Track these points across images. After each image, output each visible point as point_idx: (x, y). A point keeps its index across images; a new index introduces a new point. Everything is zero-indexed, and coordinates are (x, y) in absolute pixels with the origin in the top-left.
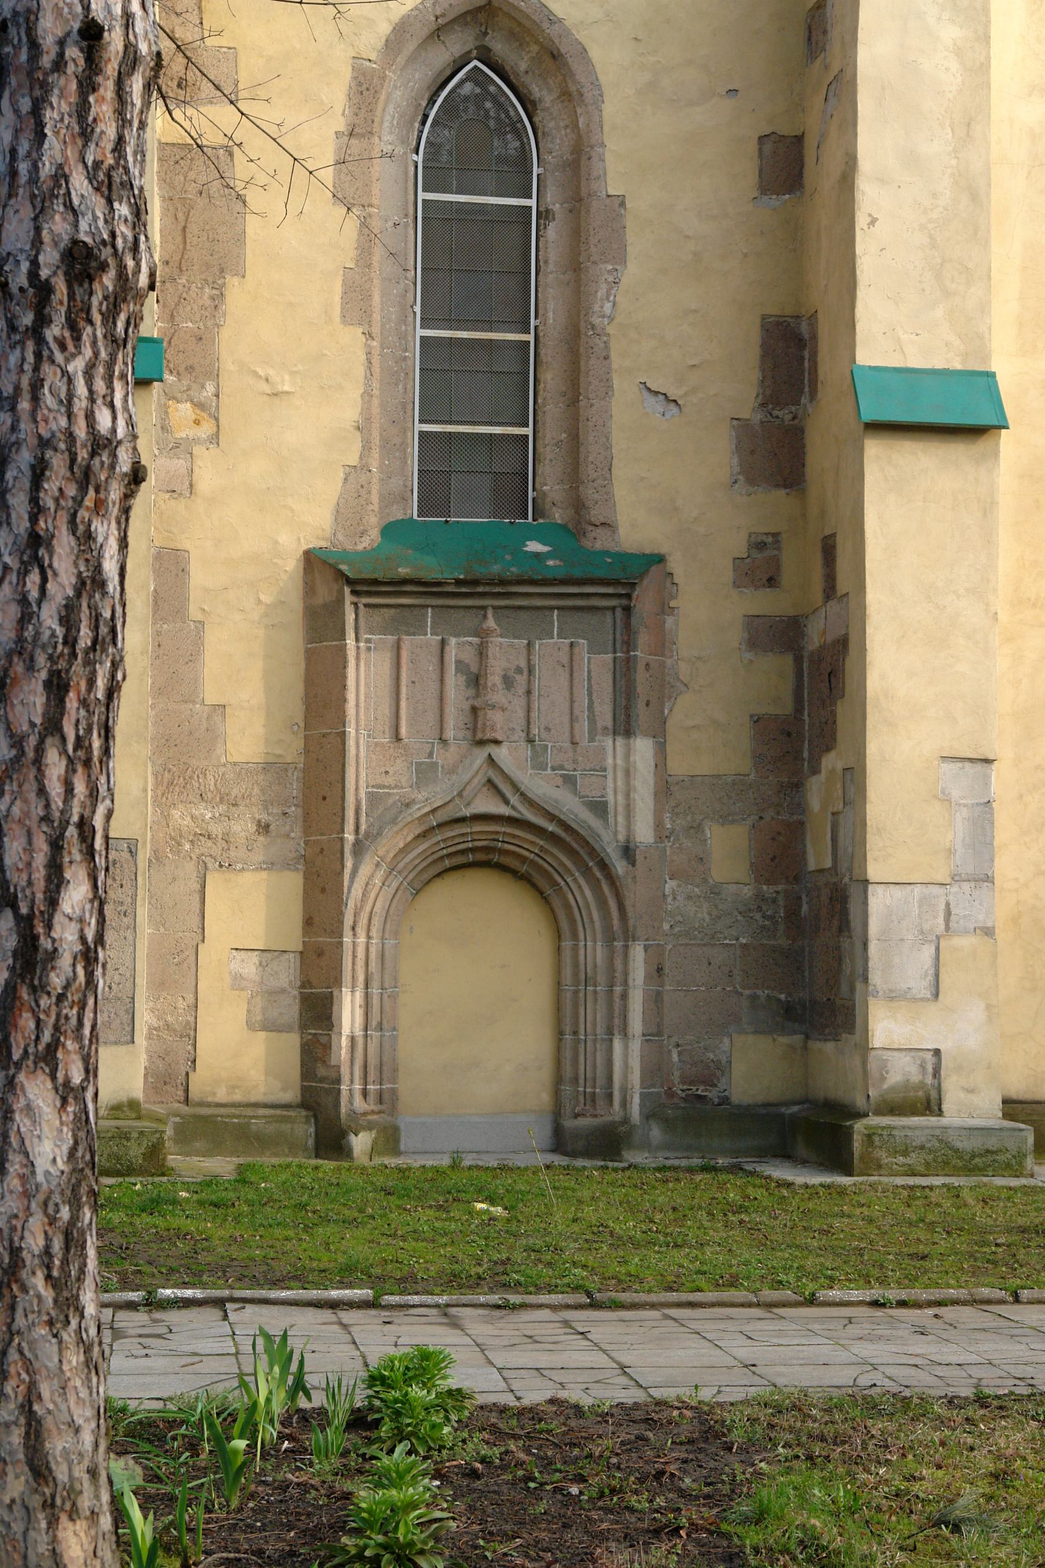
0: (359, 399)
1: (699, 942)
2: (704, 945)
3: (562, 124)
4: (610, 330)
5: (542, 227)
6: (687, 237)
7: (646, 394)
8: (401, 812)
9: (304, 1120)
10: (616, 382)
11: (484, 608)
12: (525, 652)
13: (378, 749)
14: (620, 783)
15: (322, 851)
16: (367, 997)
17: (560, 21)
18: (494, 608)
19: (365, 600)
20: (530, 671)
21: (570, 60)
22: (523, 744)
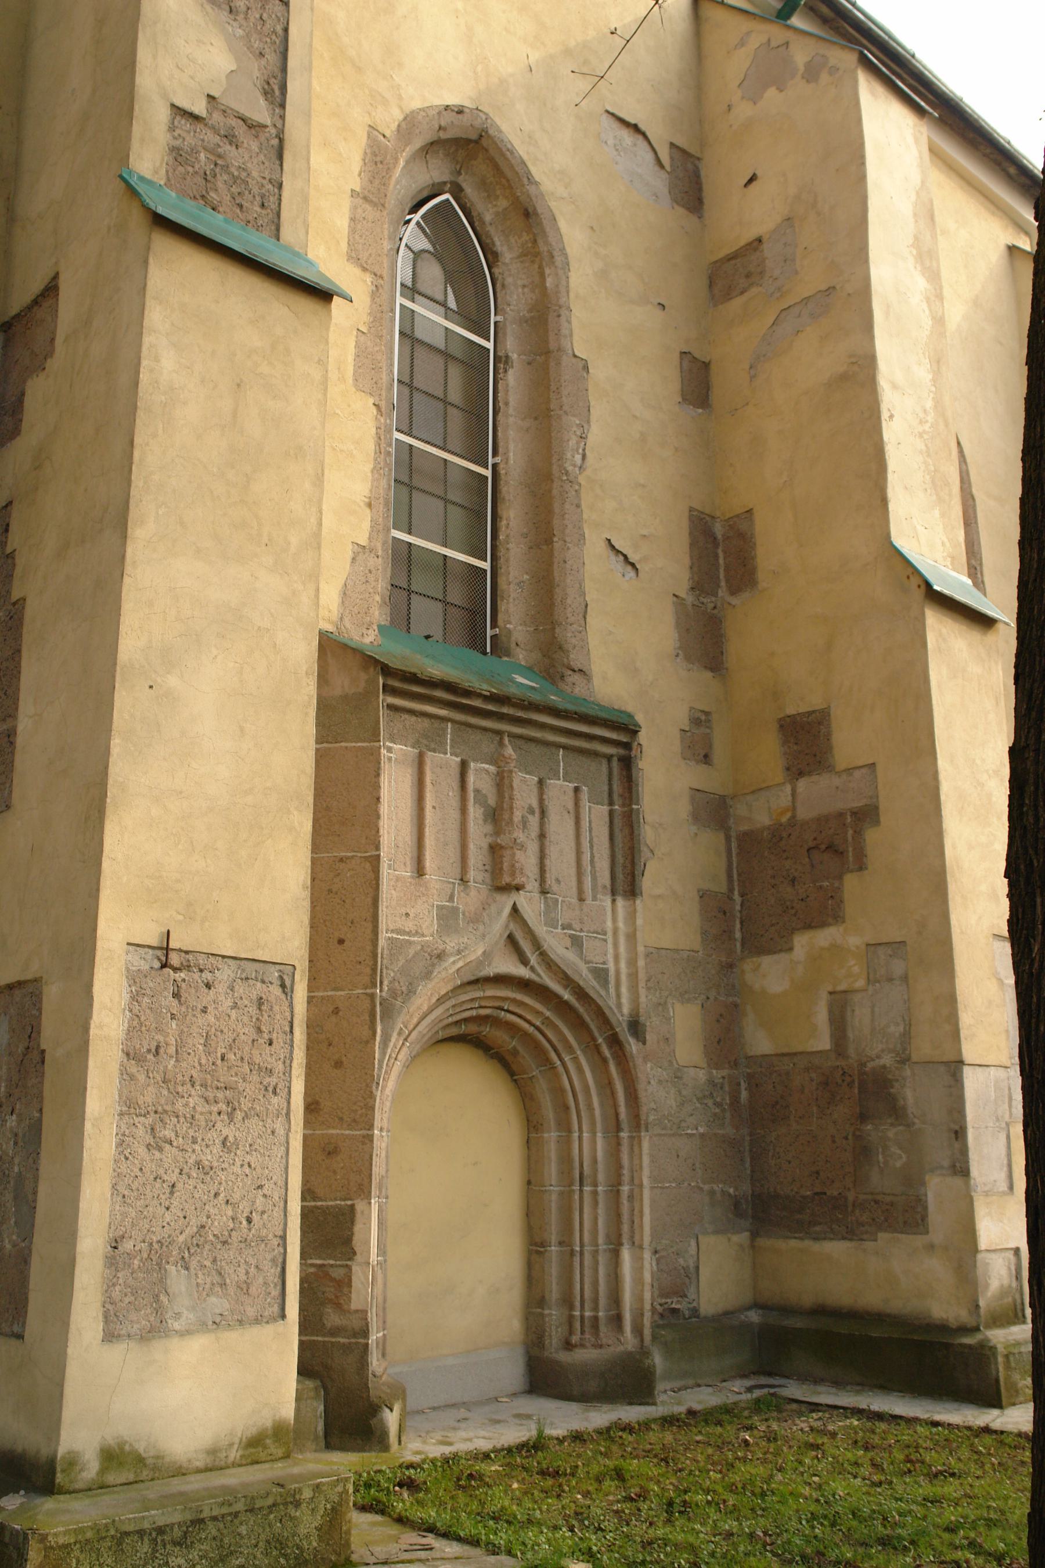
0: (370, 474)
1: (670, 1132)
2: (673, 1135)
3: (520, 283)
4: (582, 479)
5: (501, 371)
6: (634, 416)
8: (433, 965)
9: (312, 1394)
11: (499, 733)
12: (535, 790)
13: (399, 884)
14: (622, 949)
15: (336, 1011)
20: (543, 813)
21: (545, 222)
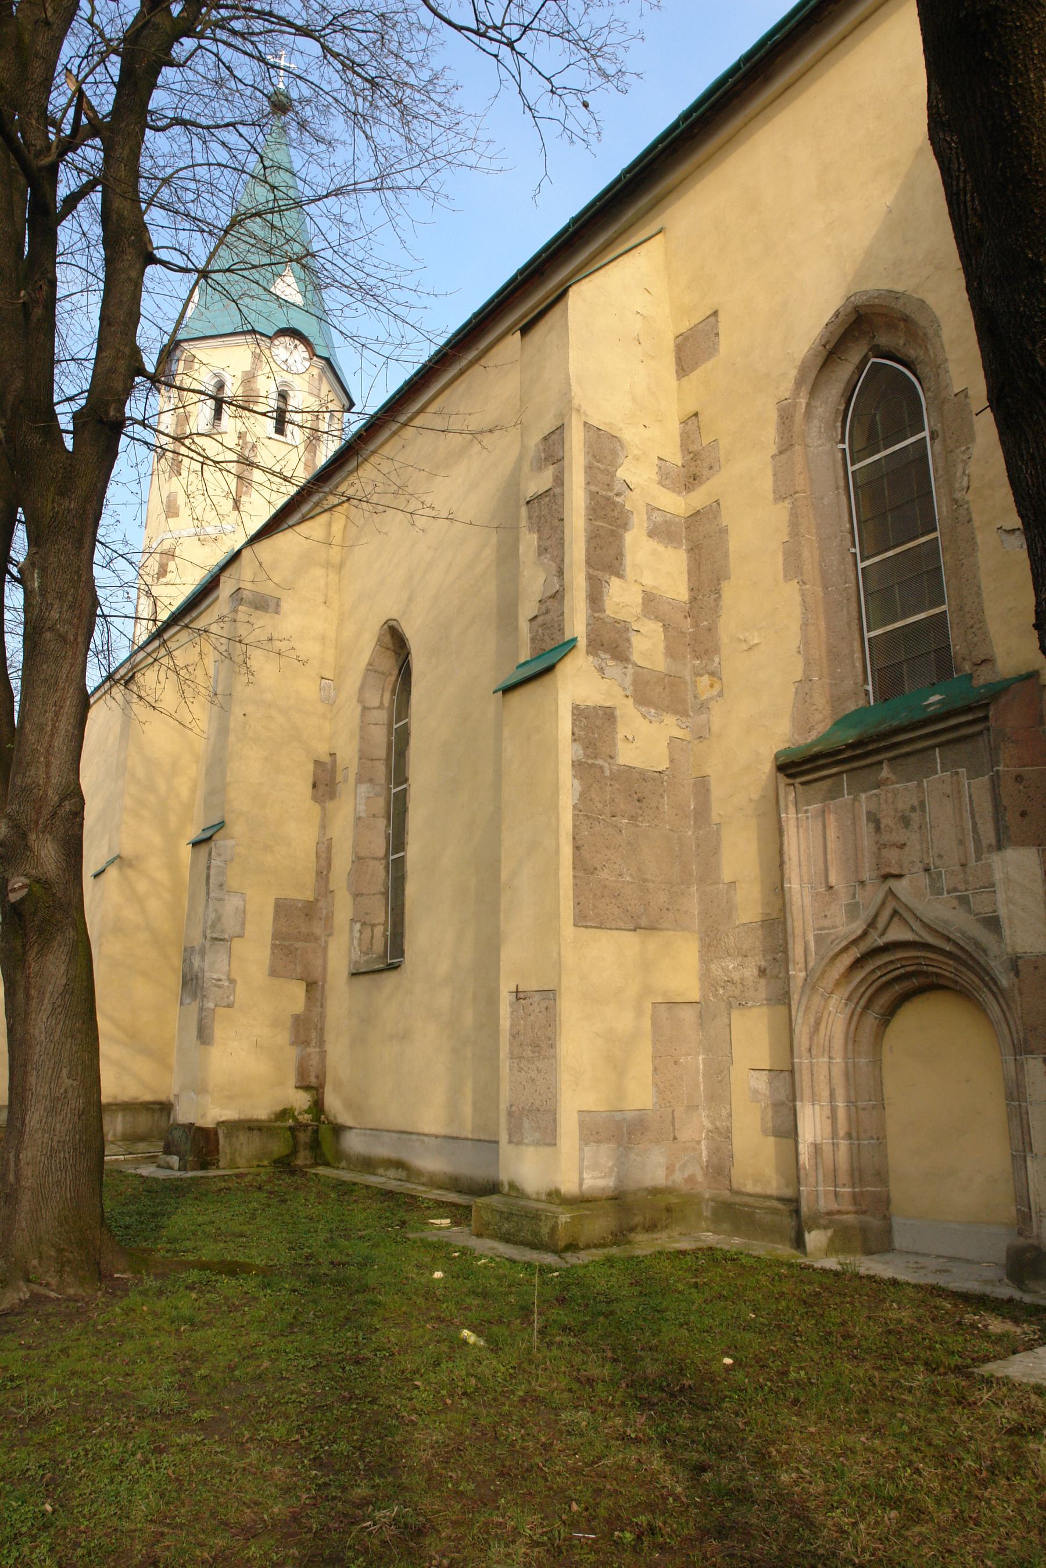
4: (969, 497)
7: (1005, 536)
10: (979, 539)
16: (833, 1110)
17: (903, 294)
18: (889, 760)
19: (798, 780)
20: (923, 810)
22: (922, 873)
